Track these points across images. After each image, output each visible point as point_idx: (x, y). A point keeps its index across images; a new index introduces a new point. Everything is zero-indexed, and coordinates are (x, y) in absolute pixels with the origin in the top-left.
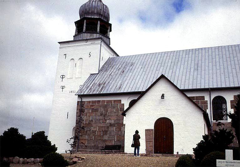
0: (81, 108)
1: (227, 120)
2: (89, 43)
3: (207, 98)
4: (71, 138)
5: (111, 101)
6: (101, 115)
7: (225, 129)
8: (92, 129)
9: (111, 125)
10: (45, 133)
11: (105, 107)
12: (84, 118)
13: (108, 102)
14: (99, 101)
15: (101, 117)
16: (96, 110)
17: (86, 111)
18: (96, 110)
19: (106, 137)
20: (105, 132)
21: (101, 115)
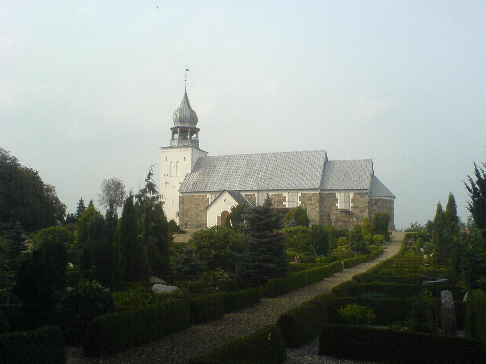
0: (182, 201)
1: (370, 199)
2: (183, 149)
3: (256, 195)
4: (152, 177)
5: (201, 196)
6: (195, 204)
7: (444, 208)
8: (190, 214)
9: (201, 211)
10: (234, 207)
11: (197, 200)
12: (185, 207)
13: (199, 196)
14: (193, 196)
15: (195, 206)
16: (192, 202)
17: (185, 202)
18: (192, 202)
19: (199, 219)
20: (198, 216)
21: (195, 204)
